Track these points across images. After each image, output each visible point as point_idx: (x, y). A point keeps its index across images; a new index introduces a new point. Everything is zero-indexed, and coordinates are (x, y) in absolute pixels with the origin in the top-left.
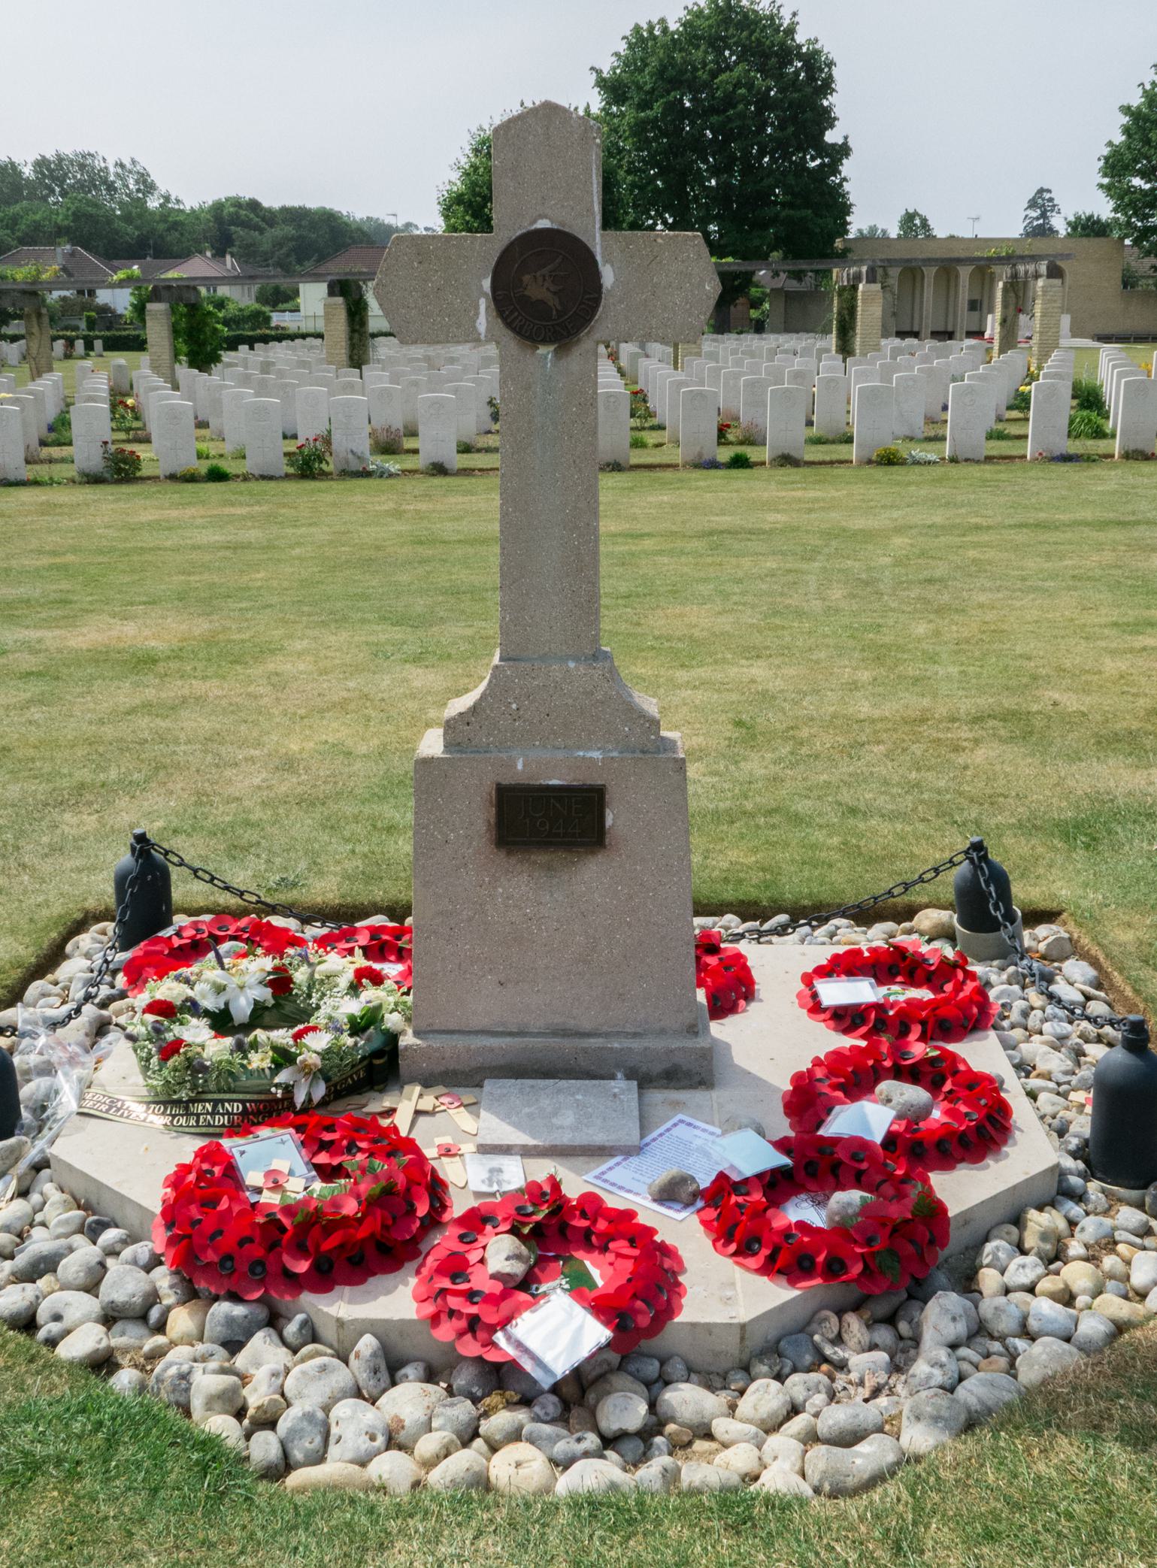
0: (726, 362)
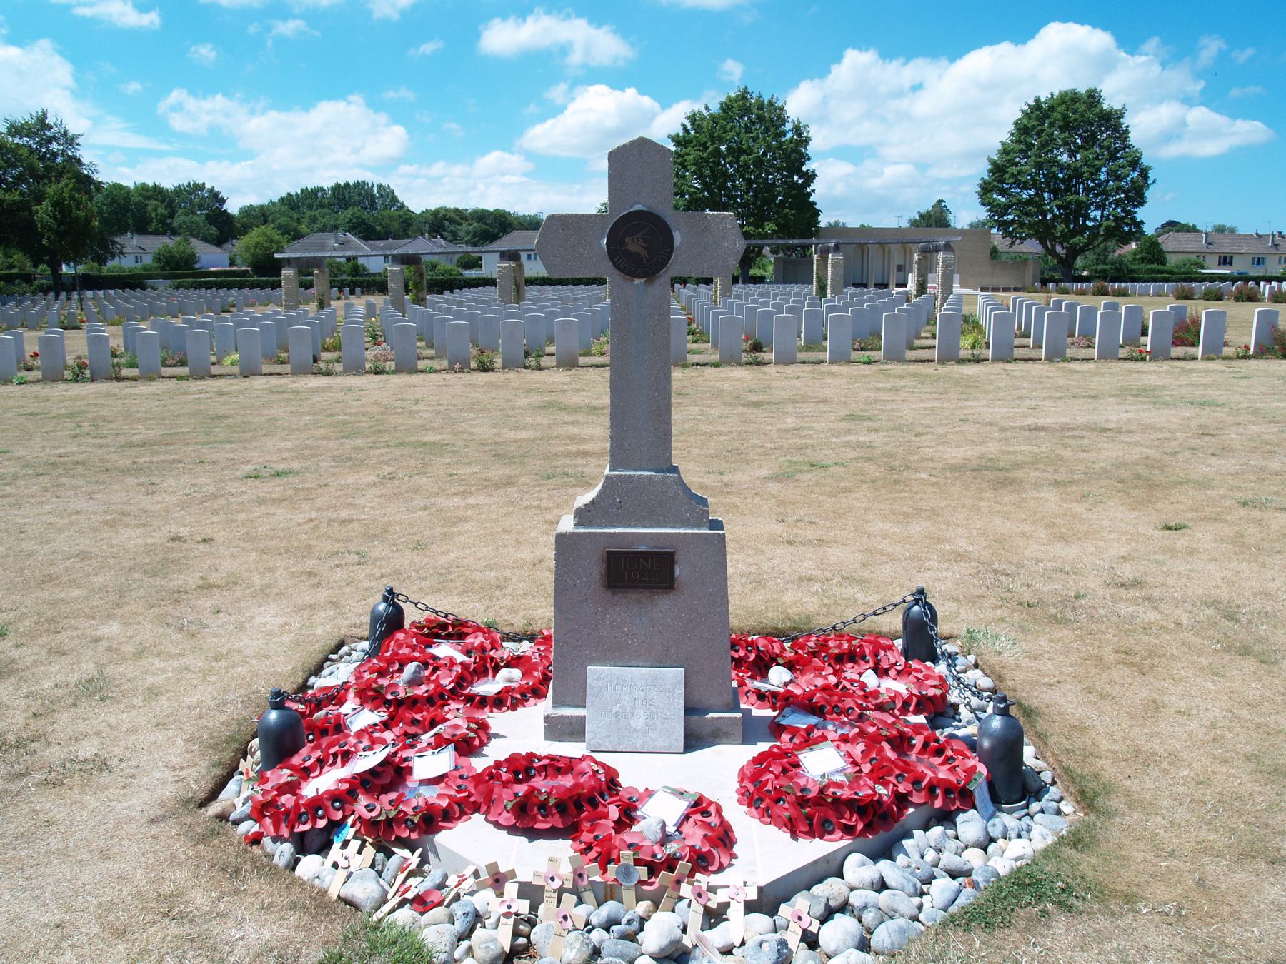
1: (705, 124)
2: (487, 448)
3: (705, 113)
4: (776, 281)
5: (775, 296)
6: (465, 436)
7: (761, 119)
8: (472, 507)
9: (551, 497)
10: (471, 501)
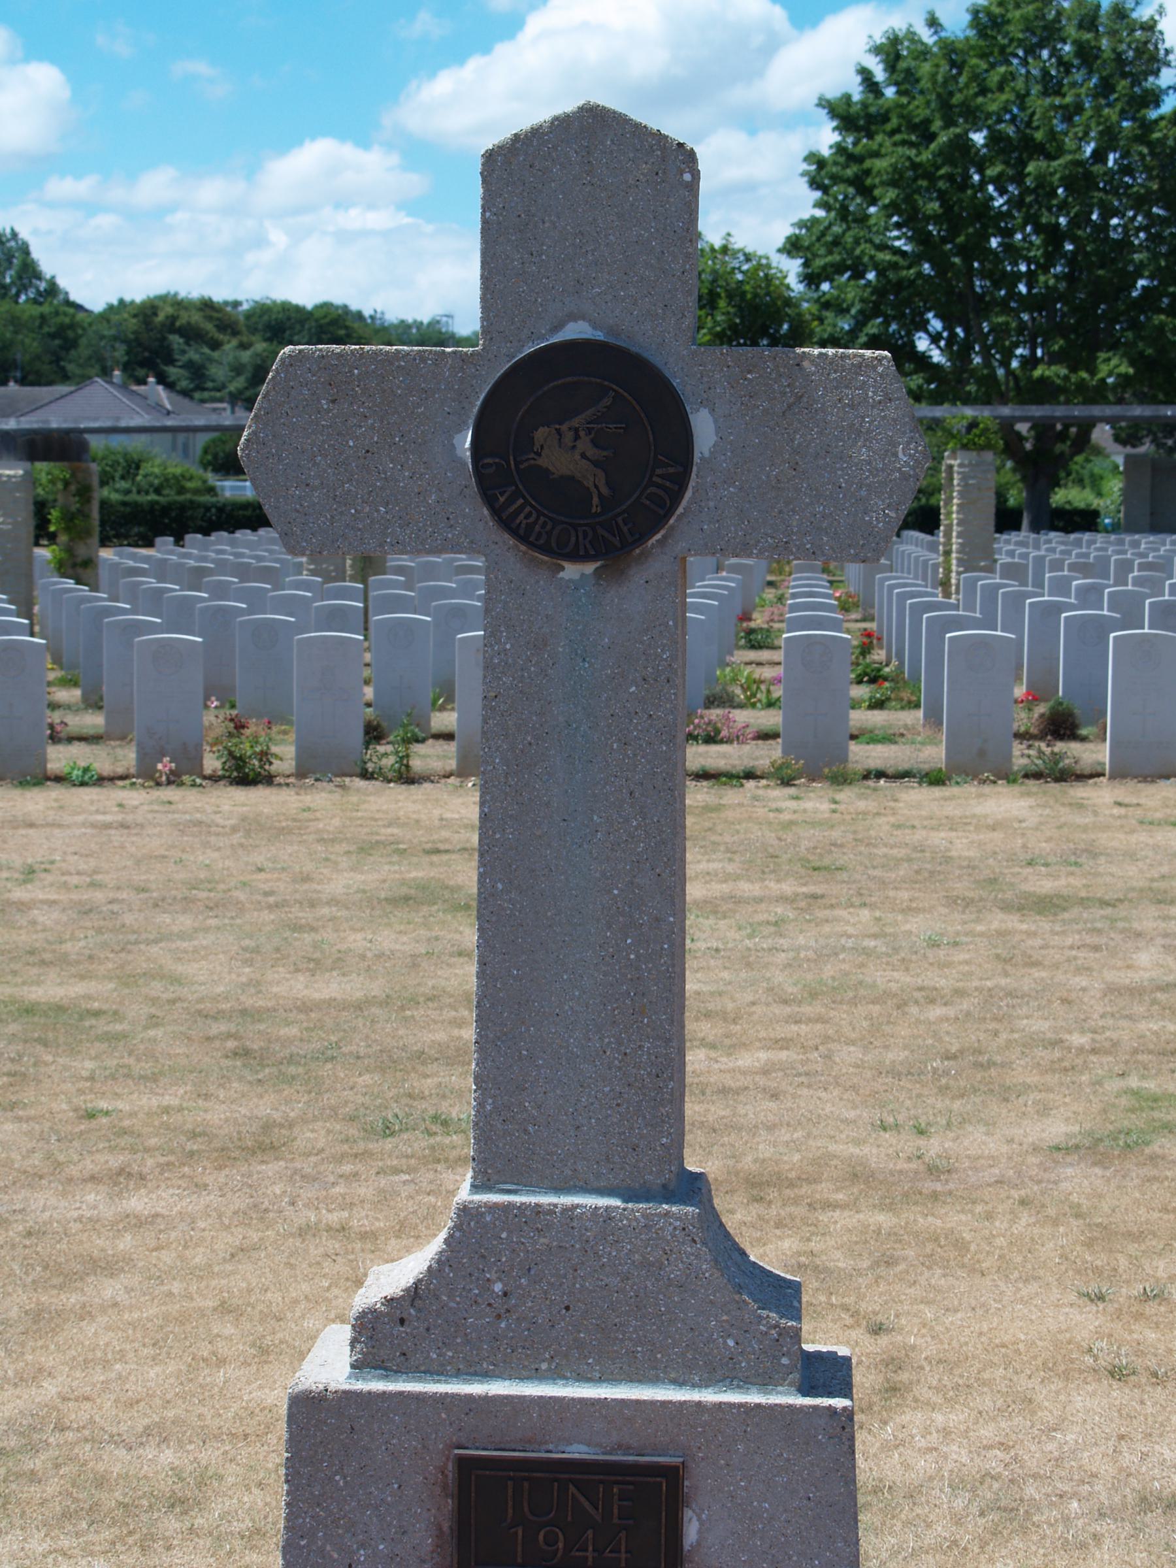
0: (1039, 584)
1: (926, 68)
2: (217, 1028)
3: (927, 36)
4: (1128, 525)
5: (1125, 567)
6: (156, 988)
7: (1087, 55)
8: (139, 1223)
9: (385, 1198)
10: (137, 1203)
